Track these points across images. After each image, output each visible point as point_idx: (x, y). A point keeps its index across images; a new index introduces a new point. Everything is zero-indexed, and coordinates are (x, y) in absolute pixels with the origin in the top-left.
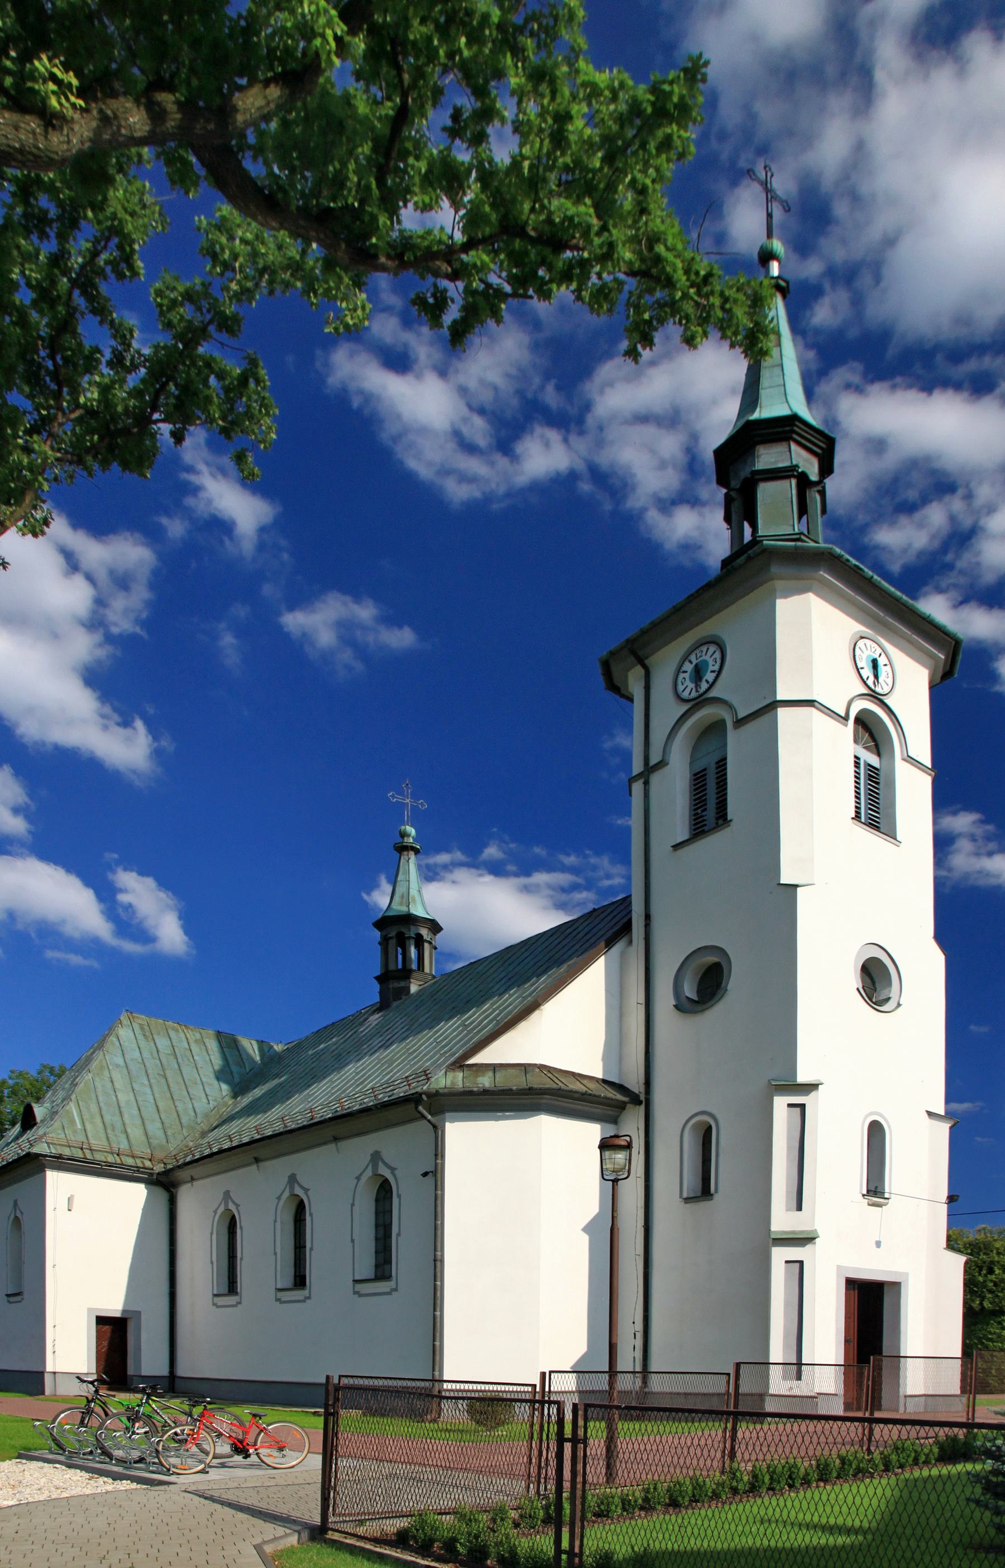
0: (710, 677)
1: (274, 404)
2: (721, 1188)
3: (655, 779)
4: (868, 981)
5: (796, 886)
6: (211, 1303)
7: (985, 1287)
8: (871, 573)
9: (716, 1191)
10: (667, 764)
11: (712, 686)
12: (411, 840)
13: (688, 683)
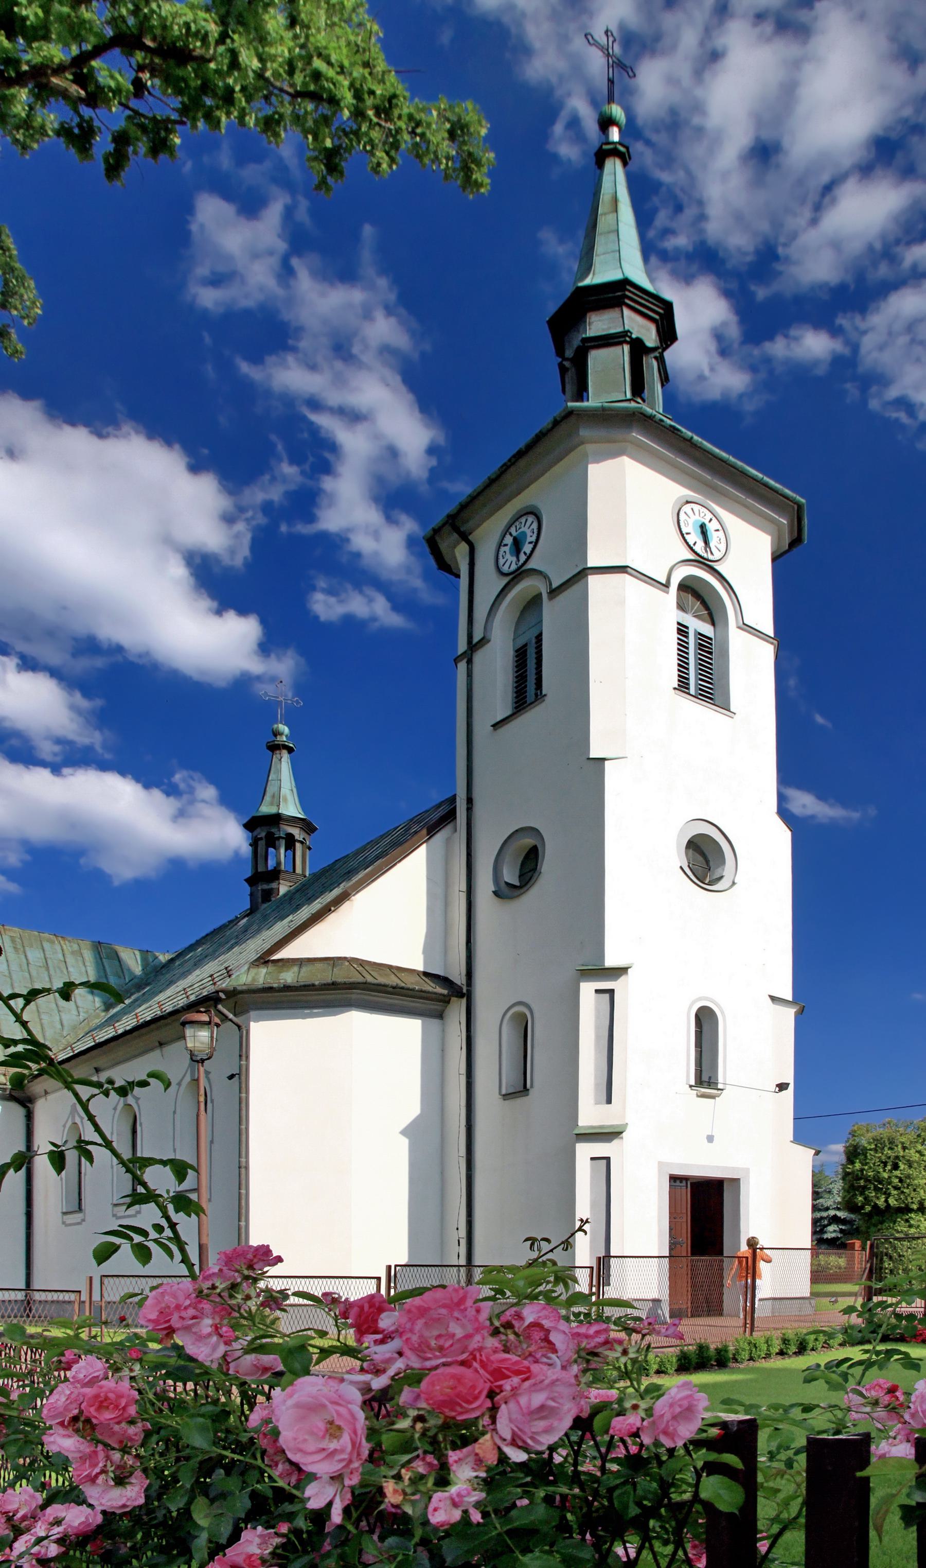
0: (527, 548)
1: (26, 275)
2: (536, 1084)
3: (478, 657)
4: (700, 858)
5: (603, 760)
6: (61, 1222)
7: (890, 1183)
8: (689, 434)
9: (532, 1086)
10: (489, 641)
11: (529, 557)
12: (285, 739)
13: (508, 556)
